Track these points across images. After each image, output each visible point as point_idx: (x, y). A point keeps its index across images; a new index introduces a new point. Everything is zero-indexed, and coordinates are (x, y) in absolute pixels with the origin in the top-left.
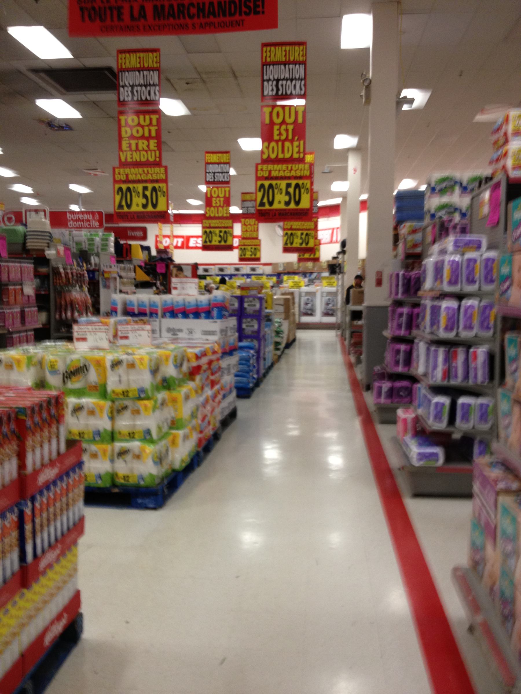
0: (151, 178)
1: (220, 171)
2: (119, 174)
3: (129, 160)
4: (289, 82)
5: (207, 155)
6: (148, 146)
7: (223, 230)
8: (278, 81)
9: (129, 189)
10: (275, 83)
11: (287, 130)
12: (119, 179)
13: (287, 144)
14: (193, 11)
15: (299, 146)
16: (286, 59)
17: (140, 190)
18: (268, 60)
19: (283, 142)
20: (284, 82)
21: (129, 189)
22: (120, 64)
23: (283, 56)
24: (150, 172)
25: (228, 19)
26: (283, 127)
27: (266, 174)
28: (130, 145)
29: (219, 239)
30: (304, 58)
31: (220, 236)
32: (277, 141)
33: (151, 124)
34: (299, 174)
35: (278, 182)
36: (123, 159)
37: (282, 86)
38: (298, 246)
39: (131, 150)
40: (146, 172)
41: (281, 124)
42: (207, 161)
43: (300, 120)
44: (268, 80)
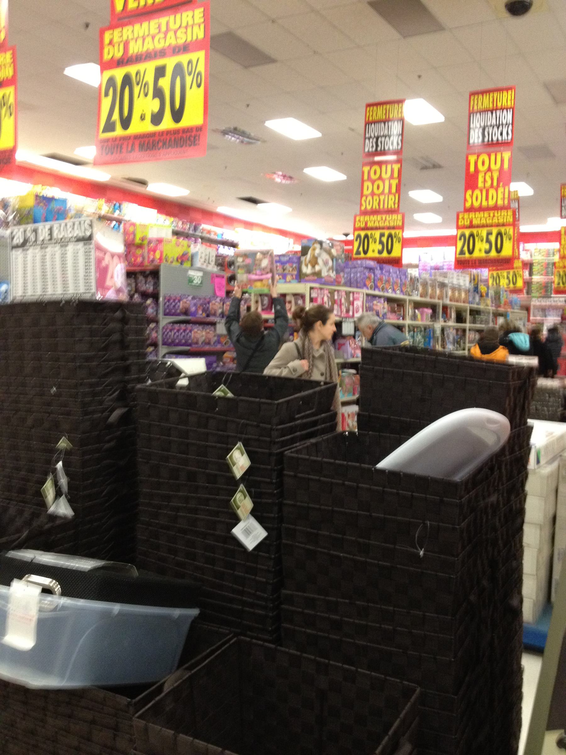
7: (387, 233)
8: (377, 139)
10: (375, 140)
13: (492, 192)
16: (386, 117)
18: (371, 119)
20: (383, 139)
22: (471, 109)
26: (489, 174)
27: (363, 225)
29: (380, 247)
31: (381, 242)
34: (392, 224)
35: (373, 232)
43: (506, 166)
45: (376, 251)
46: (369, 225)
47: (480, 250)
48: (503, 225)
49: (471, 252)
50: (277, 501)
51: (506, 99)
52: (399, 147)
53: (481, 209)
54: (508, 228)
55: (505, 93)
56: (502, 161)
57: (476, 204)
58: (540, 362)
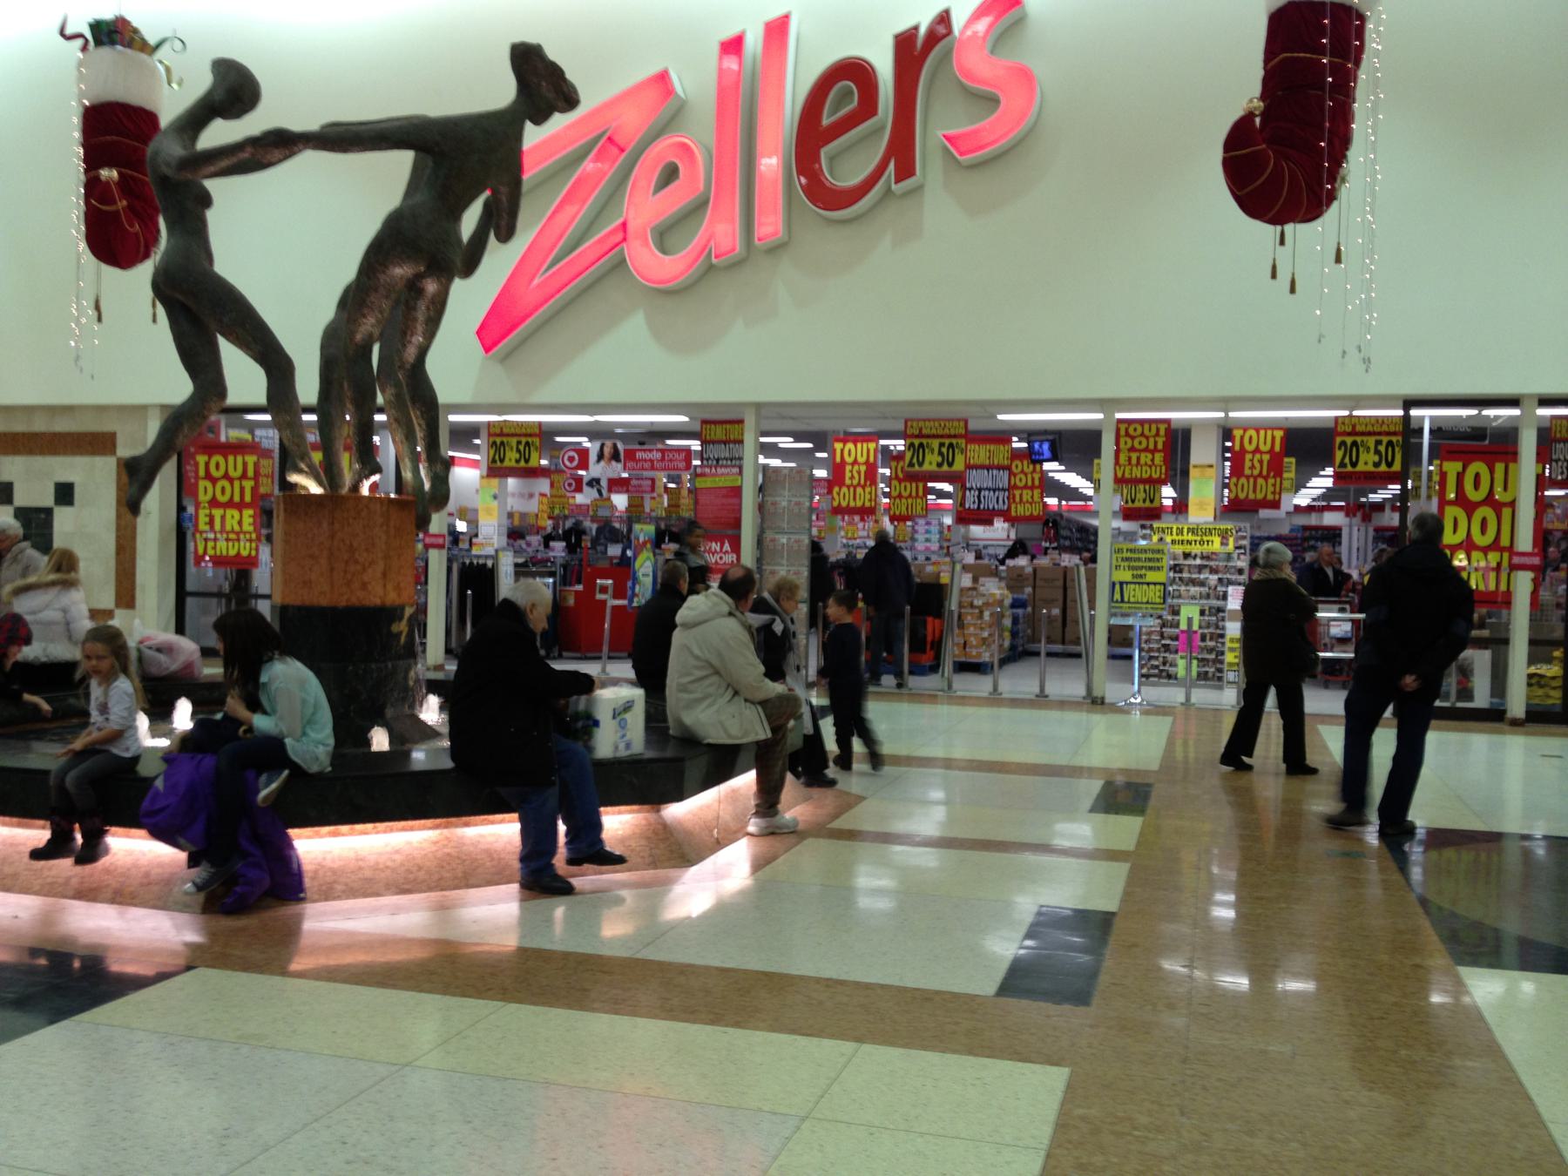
3: (1127, 475)
4: (992, 493)
6: (1153, 460)
7: (524, 440)
11: (1261, 462)
13: (859, 490)
17: (1372, 445)
19: (1255, 478)
20: (987, 492)
27: (917, 432)
30: (873, 504)
32: (1248, 477)
33: (1157, 434)
34: (952, 432)
35: (930, 441)
36: (1120, 475)
39: (1130, 464)
44: (970, 490)
45: (1371, 463)
46: (925, 431)
47: (510, 460)
48: (955, 436)
49: (1354, 465)
52: (1006, 507)
54: (960, 441)
58: (380, 754)
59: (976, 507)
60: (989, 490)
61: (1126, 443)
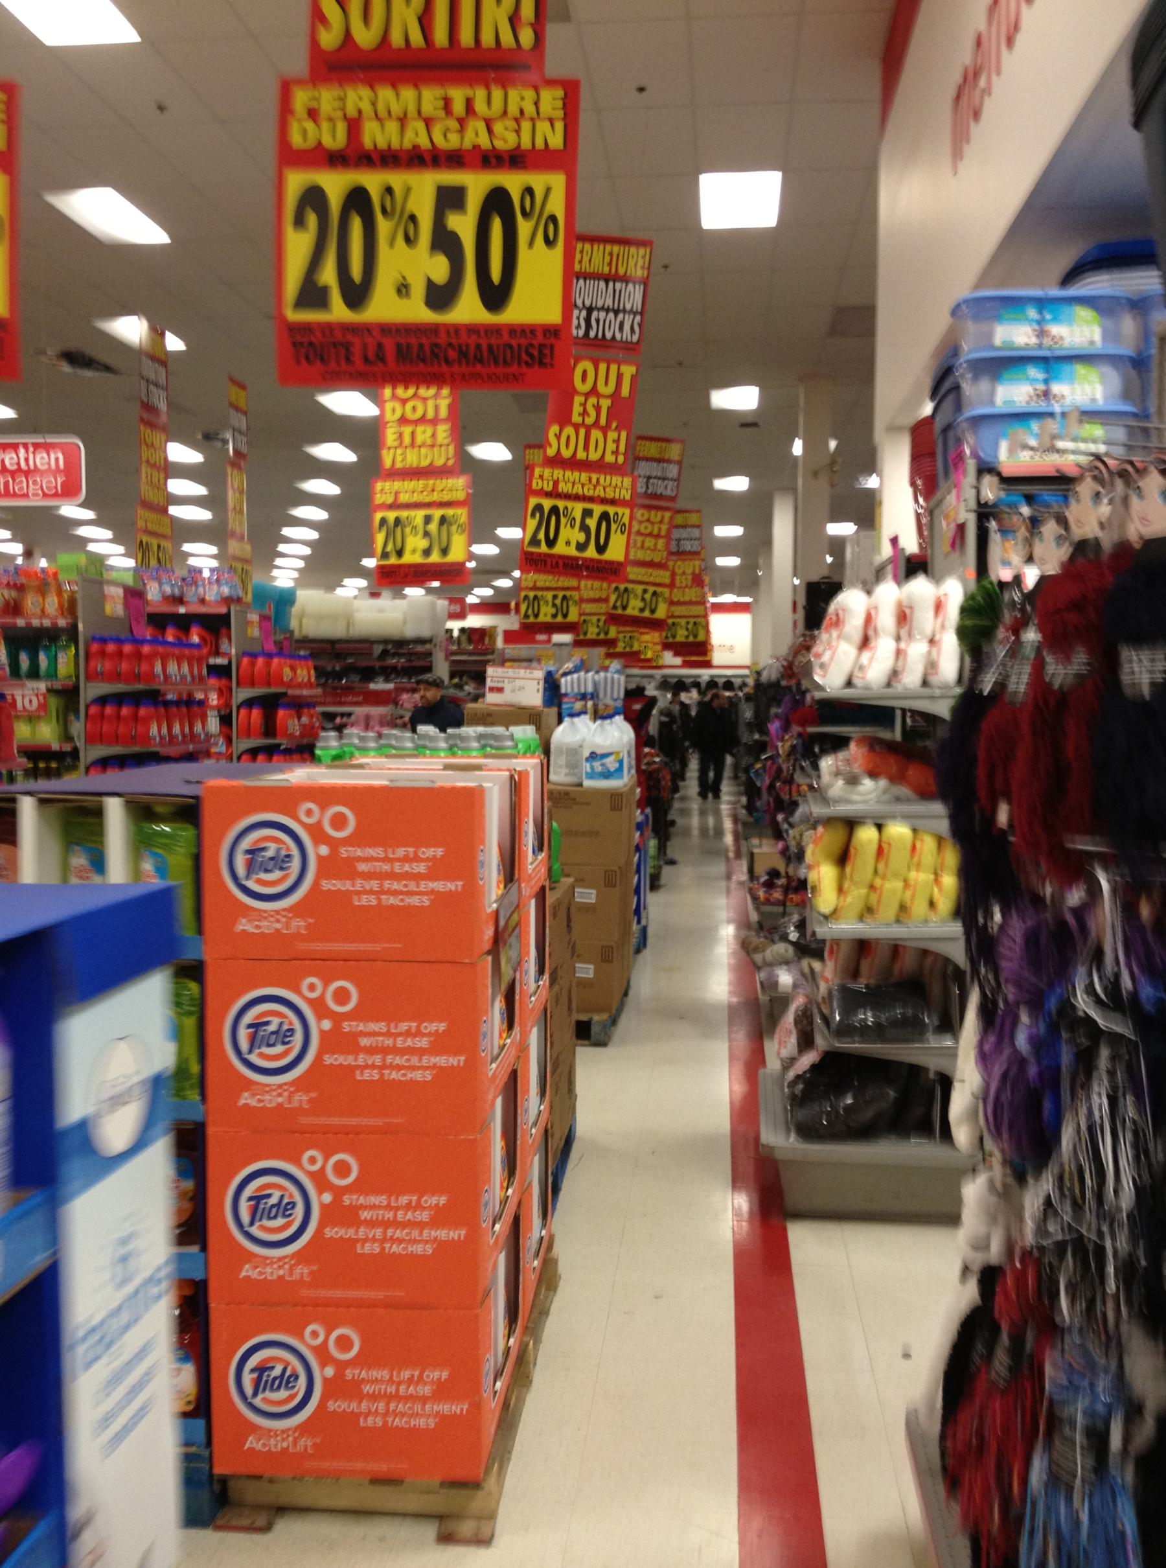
0: (484, 141)
1: (659, 474)
2: (313, 114)
4: (611, 315)
5: (639, 442)
6: (434, 435)
8: (590, 310)
9: (357, 199)
10: (584, 313)
11: (598, 408)
12: (311, 143)
13: (596, 434)
14: (453, 354)
15: (617, 442)
16: (610, 270)
17: (423, 205)
20: (602, 315)
21: (357, 199)
23: (605, 264)
24: (480, 106)
25: (500, 370)
26: (592, 400)
28: (401, 436)
32: (577, 427)
34: (610, 494)
37: (598, 321)
38: (594, 637)
40: (459, 108)
41: (587, 395)
42: (637, 454)
43: (625, 391)
50: (1047, 1261)
51: (635, 262)
52: (635, 338)
53: (573, 464)
55: (633, 250)
56: (620, 377)
57: (566, 453)
59: (581, 333)
60: (608, 310)
61: (394, 411)
